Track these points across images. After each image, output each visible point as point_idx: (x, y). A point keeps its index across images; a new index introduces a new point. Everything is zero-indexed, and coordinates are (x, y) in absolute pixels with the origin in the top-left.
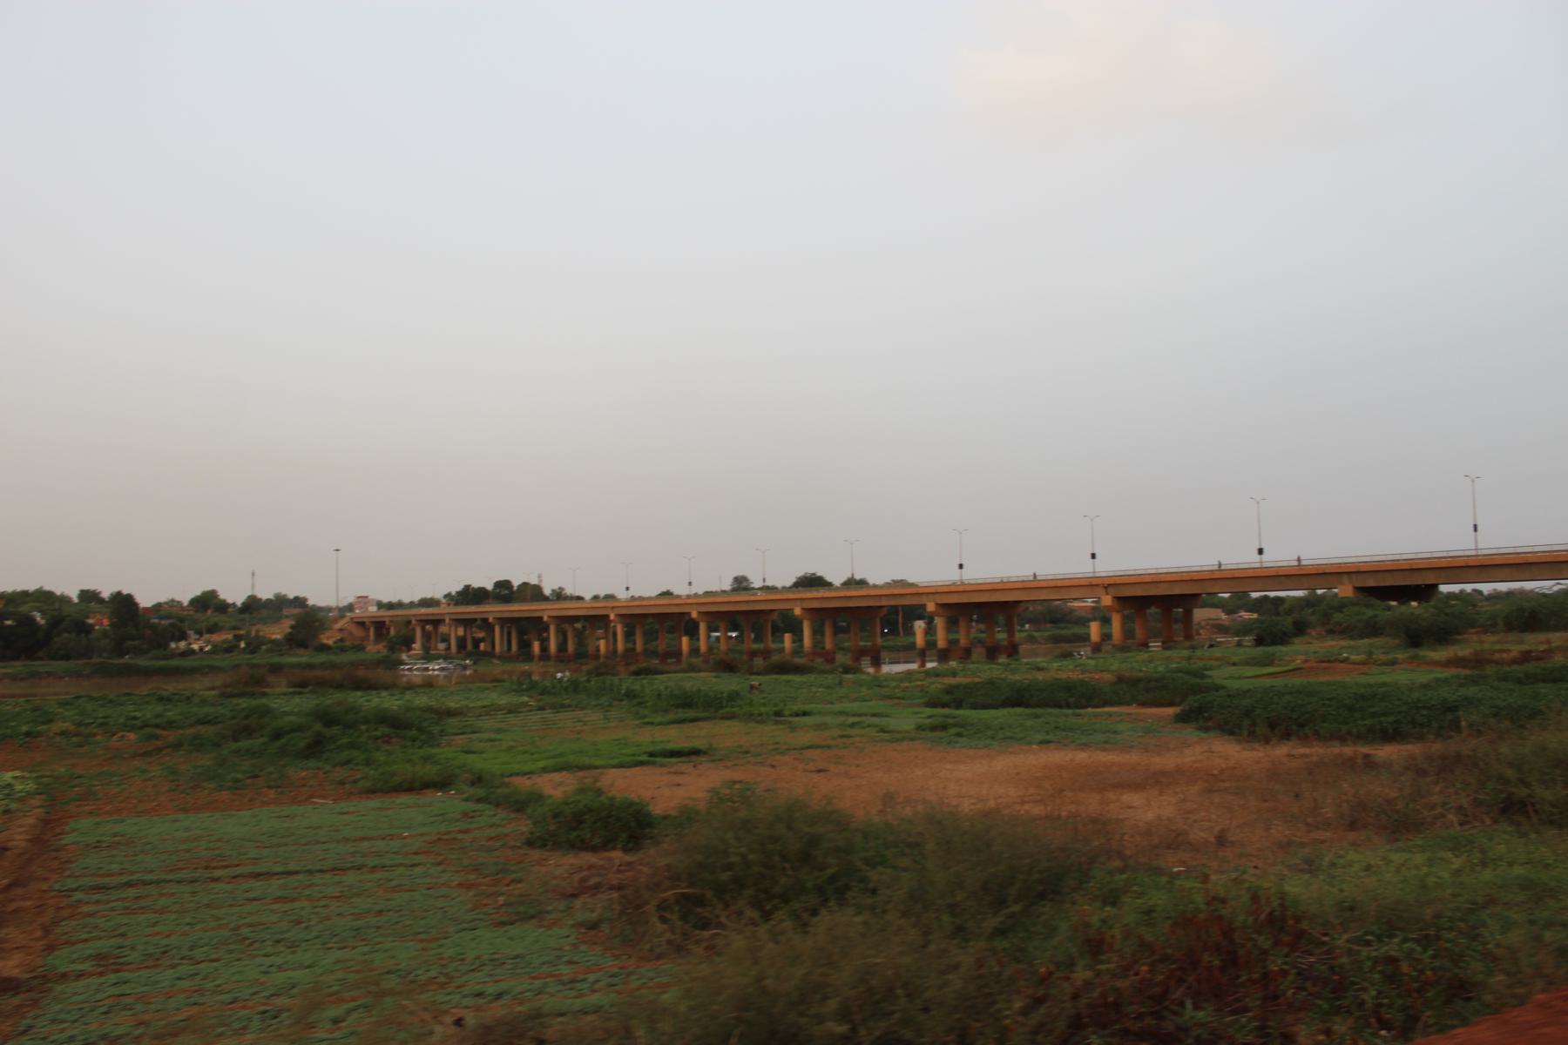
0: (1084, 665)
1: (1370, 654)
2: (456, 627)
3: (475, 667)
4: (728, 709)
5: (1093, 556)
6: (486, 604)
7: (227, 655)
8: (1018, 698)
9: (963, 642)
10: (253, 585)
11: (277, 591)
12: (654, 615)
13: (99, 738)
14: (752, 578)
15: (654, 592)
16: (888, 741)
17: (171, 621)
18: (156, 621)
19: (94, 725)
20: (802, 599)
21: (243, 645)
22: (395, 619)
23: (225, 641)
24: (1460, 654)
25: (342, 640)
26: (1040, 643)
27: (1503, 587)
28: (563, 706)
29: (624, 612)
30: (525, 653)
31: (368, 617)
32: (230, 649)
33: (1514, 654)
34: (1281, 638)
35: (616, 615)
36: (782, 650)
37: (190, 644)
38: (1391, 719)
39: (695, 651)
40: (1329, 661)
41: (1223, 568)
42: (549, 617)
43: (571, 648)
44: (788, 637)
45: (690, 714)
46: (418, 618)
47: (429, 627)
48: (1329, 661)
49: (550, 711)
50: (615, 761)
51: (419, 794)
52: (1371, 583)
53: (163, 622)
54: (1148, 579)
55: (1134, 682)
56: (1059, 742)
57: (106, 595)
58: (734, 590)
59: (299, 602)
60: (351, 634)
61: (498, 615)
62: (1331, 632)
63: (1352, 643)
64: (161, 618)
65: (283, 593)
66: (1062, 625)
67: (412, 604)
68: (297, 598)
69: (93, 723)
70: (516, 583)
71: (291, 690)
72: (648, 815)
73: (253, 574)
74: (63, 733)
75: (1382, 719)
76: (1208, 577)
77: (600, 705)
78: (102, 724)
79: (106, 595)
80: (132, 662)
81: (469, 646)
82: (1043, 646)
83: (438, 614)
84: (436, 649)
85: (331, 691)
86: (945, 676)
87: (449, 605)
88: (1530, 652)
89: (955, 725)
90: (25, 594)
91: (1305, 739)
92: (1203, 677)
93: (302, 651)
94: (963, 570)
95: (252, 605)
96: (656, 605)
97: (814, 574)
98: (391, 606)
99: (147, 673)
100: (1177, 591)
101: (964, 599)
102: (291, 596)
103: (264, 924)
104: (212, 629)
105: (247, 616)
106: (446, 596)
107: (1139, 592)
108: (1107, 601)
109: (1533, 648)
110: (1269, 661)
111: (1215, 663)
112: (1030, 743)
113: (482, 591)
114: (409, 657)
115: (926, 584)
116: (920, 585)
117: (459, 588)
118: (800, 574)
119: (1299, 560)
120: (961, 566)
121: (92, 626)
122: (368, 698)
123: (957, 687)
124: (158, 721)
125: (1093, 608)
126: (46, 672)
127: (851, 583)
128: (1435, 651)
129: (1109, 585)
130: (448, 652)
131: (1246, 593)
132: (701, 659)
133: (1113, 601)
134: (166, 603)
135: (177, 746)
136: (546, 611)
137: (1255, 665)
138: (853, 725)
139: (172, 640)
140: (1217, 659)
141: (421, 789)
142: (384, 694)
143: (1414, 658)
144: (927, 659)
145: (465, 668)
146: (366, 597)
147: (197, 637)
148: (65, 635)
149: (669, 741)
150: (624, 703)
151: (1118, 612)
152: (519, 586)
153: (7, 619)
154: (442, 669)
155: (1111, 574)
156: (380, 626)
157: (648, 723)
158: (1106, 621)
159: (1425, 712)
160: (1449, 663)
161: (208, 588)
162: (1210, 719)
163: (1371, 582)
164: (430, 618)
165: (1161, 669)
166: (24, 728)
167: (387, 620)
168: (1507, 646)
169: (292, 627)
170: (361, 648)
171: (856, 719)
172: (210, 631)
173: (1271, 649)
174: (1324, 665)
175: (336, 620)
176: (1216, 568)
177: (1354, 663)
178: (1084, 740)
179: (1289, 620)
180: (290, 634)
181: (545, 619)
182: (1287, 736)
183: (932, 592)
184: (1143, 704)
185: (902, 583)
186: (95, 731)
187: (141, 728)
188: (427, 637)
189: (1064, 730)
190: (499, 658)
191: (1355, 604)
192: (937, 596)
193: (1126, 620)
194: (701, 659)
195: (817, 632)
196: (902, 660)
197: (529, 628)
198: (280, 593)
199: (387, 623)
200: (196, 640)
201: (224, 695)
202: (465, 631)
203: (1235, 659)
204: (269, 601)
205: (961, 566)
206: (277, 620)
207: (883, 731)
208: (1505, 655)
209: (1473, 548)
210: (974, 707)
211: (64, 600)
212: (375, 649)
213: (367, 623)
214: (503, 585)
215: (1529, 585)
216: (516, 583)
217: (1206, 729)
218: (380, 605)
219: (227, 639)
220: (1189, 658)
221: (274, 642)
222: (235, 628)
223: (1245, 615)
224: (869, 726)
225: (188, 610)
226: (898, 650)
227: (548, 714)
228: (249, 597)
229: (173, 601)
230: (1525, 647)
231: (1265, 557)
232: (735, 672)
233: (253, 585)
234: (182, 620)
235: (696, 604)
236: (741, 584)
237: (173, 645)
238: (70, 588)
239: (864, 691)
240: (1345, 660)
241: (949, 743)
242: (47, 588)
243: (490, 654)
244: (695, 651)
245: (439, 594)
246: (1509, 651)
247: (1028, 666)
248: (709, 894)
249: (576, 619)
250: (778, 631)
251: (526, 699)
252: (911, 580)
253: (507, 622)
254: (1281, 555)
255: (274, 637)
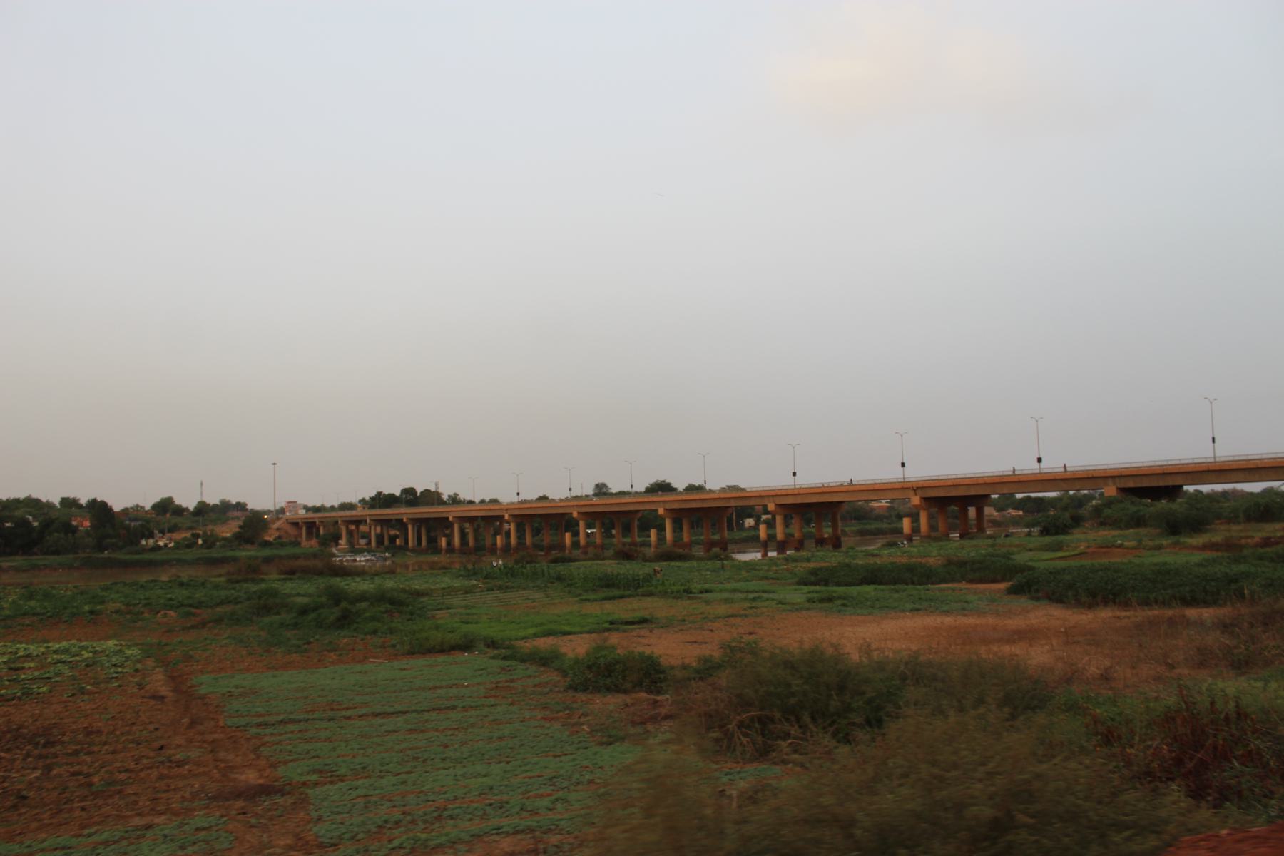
0: (908, 552)
1: (1140, 541)
2: (376, 526)
3: (393, 559)
4: (645, 589)
5: (903, 465)
6: (395, 507)
7: (189, 550)
8: (874, 577)
9: (797, 535)
10: (202, 493)
11: (222, 498)
12: (541, 516)
13: (146, 615)
14: (610, 485)
15: (535, 497)
16: (789, 611)
17: (140, 523)
18: (127, 522)
19: (140, 605)
20: (664, 502)
21: (200, 542)
22: (323, 520)
23: (185, 539)
24: (1214, 540)
25: (280, 537)
26: (850, 536)
27: (1219, 488)
28: (507, 587)
29: (516, 513)
30: (433, 547)
31: (301, 519)
32: (190, 545)
33: (1257, 539)
34: (1063, 529)
35: (510, 515)
36: (648, 545)
37: (157, 541)
38: (1187, 589)
39: (576, 544)
40: (1108, 546)
41: (1017, 473)
42: (454, 517)
43: (471, 542)
44: (653, 532)
45: (616, 592)
46: (344, 519)
47: (353, 527)
48: (1107, 547)
49: (498, 592)
50: (586, 629)
51: (449, 654)
52: (1131, 484)
53: (133, 524)
54: (949, 483)
55: (962, 564)
56: (926, 610)
57: (83, 501)
58: (595, 495)
59: (240, 507)
60: (286, 532)
61: (411, 517)
62: (1102, 524)
63: (1122, 532)
64: (131, 520)
65: (227, 499)
66: (865, 521)
67: (332, 508)
68: (238, 504)
69: (139, 604)
70: (419, 490)
71: (283, 576)
72: (659, 664)
73: (202, 484)
74: (117, 612)
75: (1181, 588)
76: (998, 481)
77: (538, 586)
78: (145, 605)
79: (83, 501)
80: (112, 556)
81: (386, 542)
82: (853, 539)
83: (310, 518)
84: (358, 544)
85: (316, 577)
86: (802, 561)
87: (364, 508)
88: (1269, 538)
89: (839, 598)
90: (17, 501)
91: (1126, 605)
92: (1009, 559)
93: (249, 546)
94: (796, 477)
95: (202, 509)
96: (543, 507)
97: (664, 481)
98: (316, 510)
99: (126, 565)
100: (973, 492)
101: (799, 500)
102: (234, 502)
103: (420, 748)
104: (173, 529)
105: (200, 519)
106: (360, 501)
107: (942, 493)
108: (916, 500)
109: (1272, 535)
110: (1059, 547)
111: (1015, 549)
112: (903, 611)
113: (392, 496)
114: (338, 550)
115: (806, 486)
116: (748, 490)
117: (373, 494)
118: (653, 481)
119: (1065, 467)
120: (794, 474)
121: (76, 528)
122: (347, 582)
123: (820, 569)
124: (190, 602)
125: (888, 507)
126: (44, 565)
127: (691, 488)
128: (1192, 537)
129: (917, 488)
130: (369, 547)
131: (1012, 495)
132: (580, 551)
133: (921, 502)
134: (131, 508)
135: (219, 621)
136: (452, 513)
137: (1047, 550)
138: (754, 599)
139: (142, 538)
140: (1017, 546)
141: (449, 651)
142: (358, 579)
143: (1176, 544)
144: (769, 549)
145: (385, 559)
146: (295, 502)
147: (161, 535)
148: (56, 534)
149: (796, 590)
150: (555, 585)
151: (924, 509)
152: (421, 493)
153: (8, 522)
154: (367, 561)
155: (919, 479)
156: (311, 526)
157: (586, 600)
158: (915, 517)
159: (1213, 583)
160: (1204, 547)
161: (166, 495)
162: (1037, 591)
163: (1131, 484)
164: (354, 519)
165: (973, 554)
166: (87, 608)
167: (300, 521)
168: (1250, 534)
169: (240, 527)
170: (297, 544)
171: (756, 595)
172: (171, 530)
173: (1061, 538)
174: (1104, 550)
175: (273, 521)
176: (1011, 473)
177: (1127, 548)
178: (946, 608)
179: (1067, 515)
180: (239, 533)
181: (451, 519)
182: (1106, 602)
183: (763, 496)
184: (972, 581)
185: (735, 488)
186: (142, 610)
187: (178, 607)
188: (350, 533)
189: (926, 600)
190: (413, 551)
191: (1121, 502)
192: (775, 498)
193: (930, 517)
194: (580, 551)
195: (677, 526)
196: (736, 551)
197: (436, 526)
198: (225, 500)
199: (317, 523)
200: (160, 538)
201: (230, 581)
202: (382, 529)
203: (1031, 546)
204: (215, 506)
205: (794, 474)
206: (225, 522)
207: (780, 603)
208: (1249, 541)
209: (1216, 455)
210: (839, 584)
211: (49, 505)
212: (310, 545)
213: (300, 524)
214: (409, 492)
215: (1239, 486)
216: (419, 490)
217: (1038, 599)
218: (306, 508)
219: (186, 537)
220: (993, 546)
221: (225, 539)
222: (191, 528)
223: (1013, 512)
224: (767, 600)
225: (150, 514)
226: (736, 543)
227: (497, 593)
228: (199, 503)
229: (138, 506)
230: (1265, 534)
231: (1043, 464)
232: (633, 560)
233: (202, 493)
234: (148, 521)
235: (577, 506)
236: (601, 490)
237: (143, 542)
238: (51, 494)
239: (744, 574)
240: (1120, 546)
241: (839, 611)
242: (34, 496)
243: (404, 548)
244: (576, 544)
245: (354, 499)
246: (1252, 537)
247: (864, 554)
248: (778, 715)
249: (474, 518)
250: (645, 528)
251: (475, 582)
252: (742, 486)
253: (420, 522)
254: (1053, 464)
255: (224, 535)
